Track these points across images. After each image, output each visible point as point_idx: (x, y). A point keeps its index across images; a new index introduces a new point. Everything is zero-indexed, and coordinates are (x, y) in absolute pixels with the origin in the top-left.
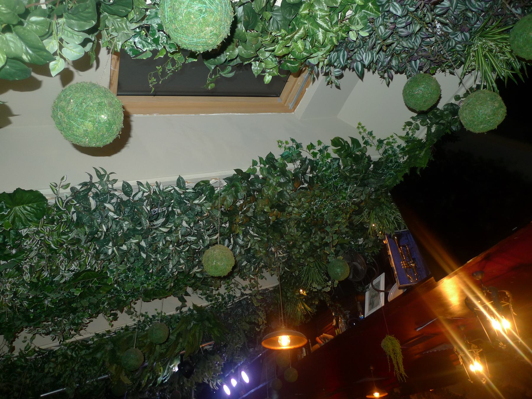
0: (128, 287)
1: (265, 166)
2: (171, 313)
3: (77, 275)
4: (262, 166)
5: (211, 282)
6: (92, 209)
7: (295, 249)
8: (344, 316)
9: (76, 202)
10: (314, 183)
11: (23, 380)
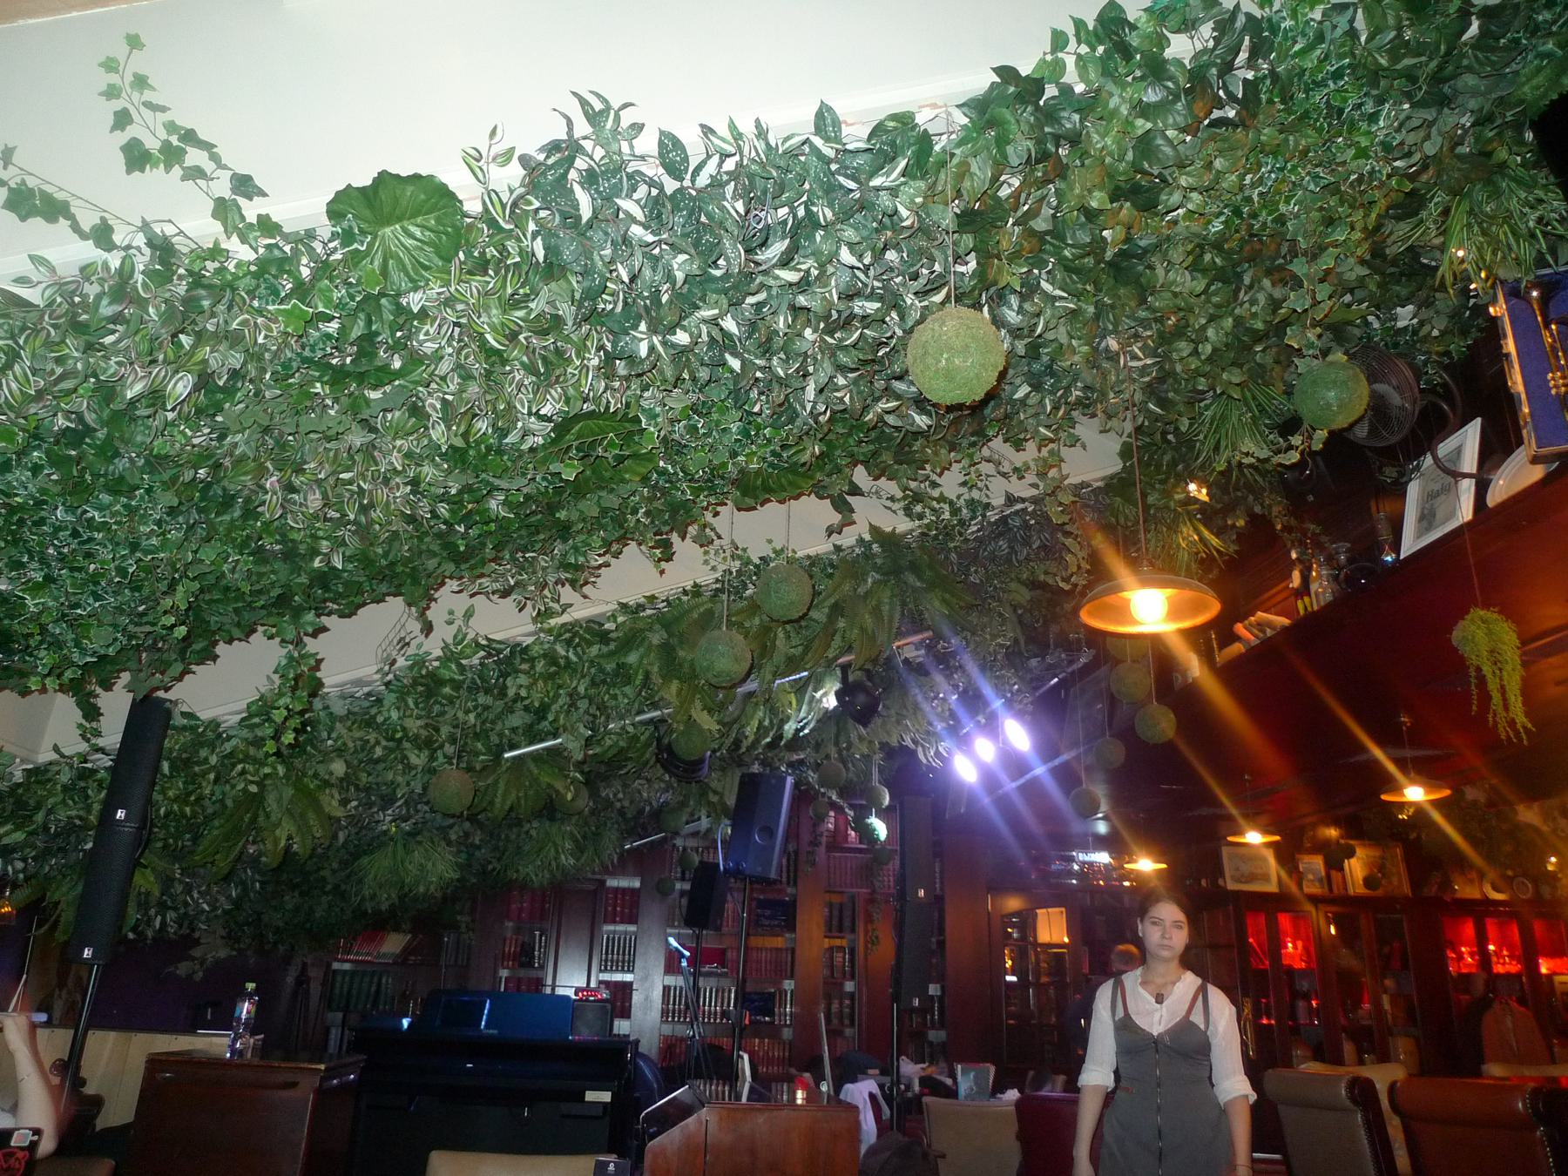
0: (697, 461)
1: (1093, 49)
2: (812, 551)
3: (563, 426)
4: (1084, 49)
5: (922, 451)
6: (584, 220)
7: (1182, 344)
8: (1330, 560)
9: (537, 204)
10: (1260, 100)
11: (460, 714)
